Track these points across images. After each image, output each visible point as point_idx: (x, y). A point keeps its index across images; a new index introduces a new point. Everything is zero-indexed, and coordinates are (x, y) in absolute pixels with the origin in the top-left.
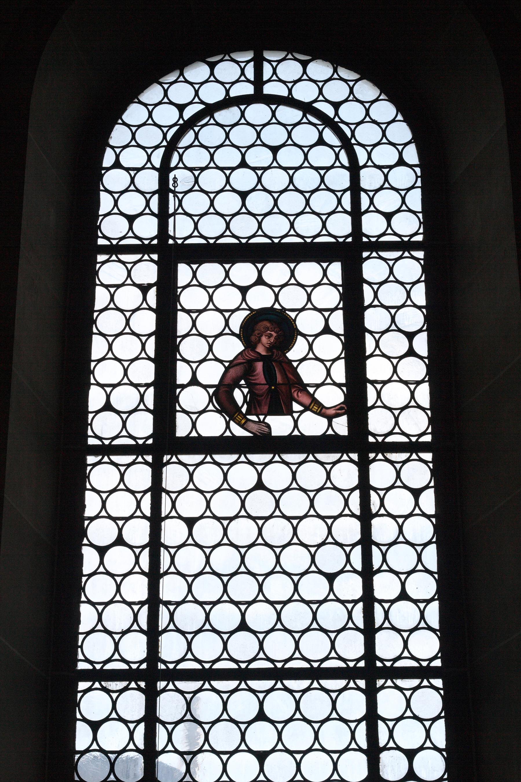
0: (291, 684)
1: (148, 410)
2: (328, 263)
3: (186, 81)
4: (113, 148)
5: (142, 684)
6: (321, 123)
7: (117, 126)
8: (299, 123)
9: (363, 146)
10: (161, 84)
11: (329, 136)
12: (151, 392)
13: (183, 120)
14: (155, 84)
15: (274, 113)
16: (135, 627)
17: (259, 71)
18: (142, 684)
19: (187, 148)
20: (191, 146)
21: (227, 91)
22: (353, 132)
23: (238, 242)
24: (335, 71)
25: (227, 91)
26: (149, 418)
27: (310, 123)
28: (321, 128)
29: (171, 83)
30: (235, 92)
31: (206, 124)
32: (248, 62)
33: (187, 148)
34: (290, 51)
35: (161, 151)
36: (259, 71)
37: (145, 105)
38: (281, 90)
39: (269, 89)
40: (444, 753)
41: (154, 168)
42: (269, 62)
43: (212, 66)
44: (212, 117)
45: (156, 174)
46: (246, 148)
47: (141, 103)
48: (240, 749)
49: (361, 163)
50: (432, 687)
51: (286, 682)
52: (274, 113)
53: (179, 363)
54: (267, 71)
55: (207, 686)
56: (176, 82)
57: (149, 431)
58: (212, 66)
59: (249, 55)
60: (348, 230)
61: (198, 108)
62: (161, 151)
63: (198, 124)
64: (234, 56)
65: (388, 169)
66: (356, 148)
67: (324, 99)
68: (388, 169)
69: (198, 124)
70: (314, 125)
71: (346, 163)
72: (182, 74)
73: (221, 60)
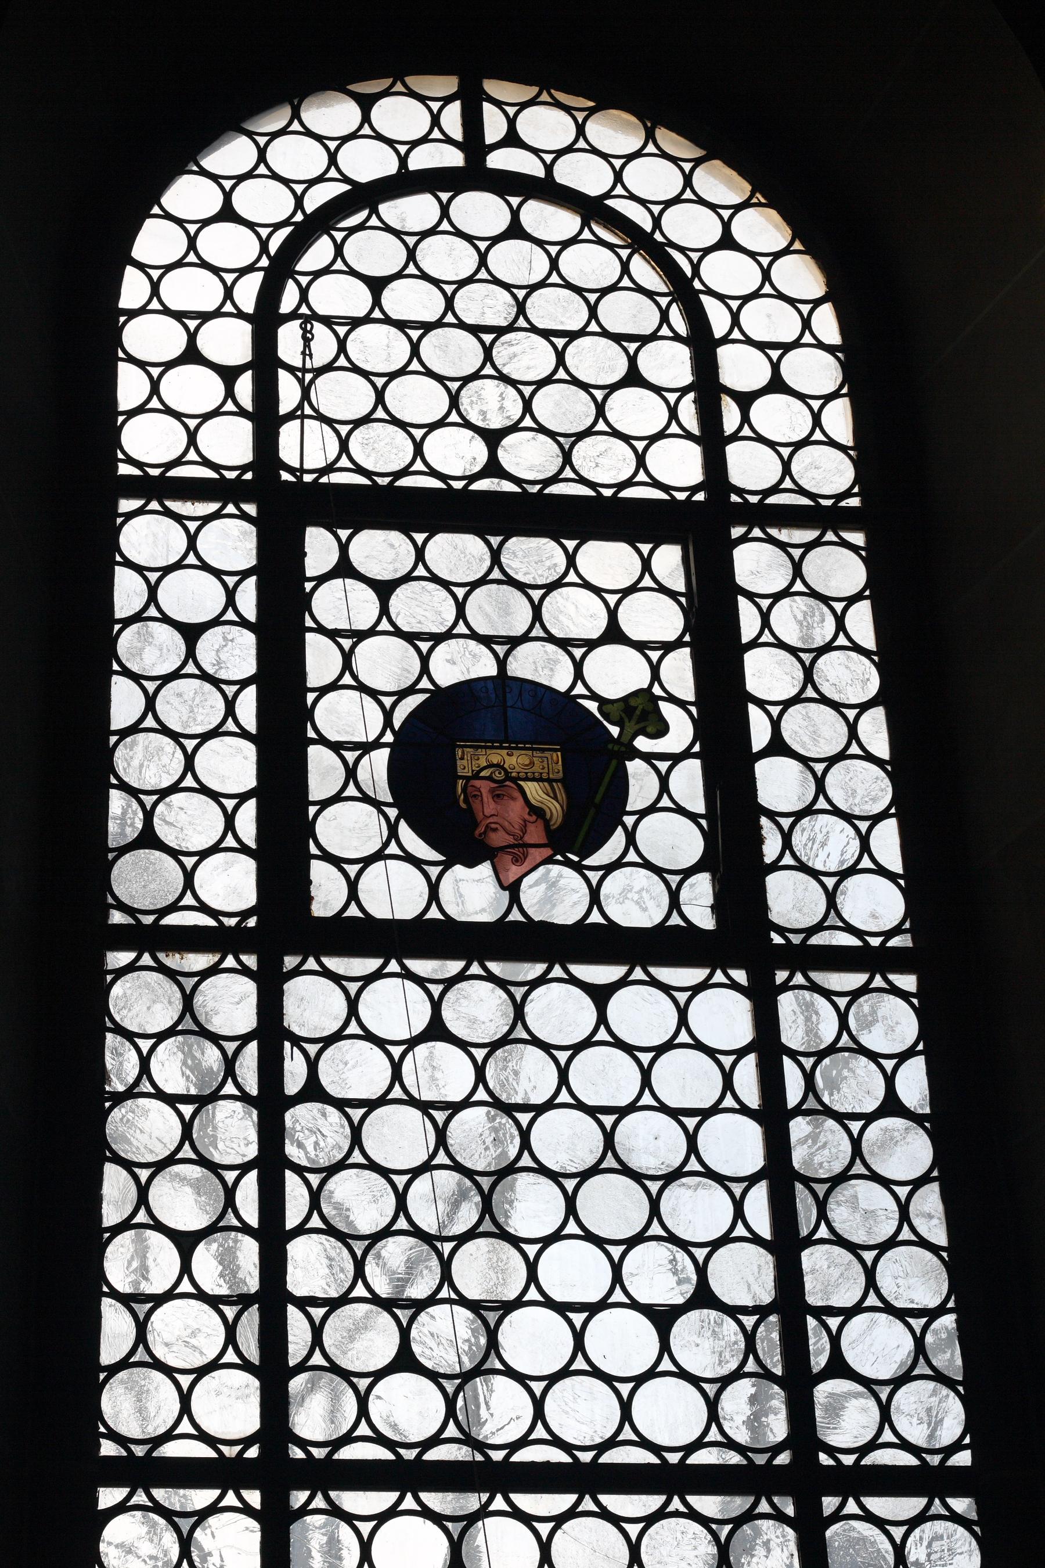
0: (617, 1503)
1: (243, 849)
2: (587, 1314)
3: (308, 133)
4: (141, 267)
5: (254, 1498)
6: (580, 701)
7: (149, 223)
8: (574, 241)
9: (721, 298)
10: (250, 135)
11: (643, 271)
12: (249, 810)
13: (304, 212)
14: (253, 562)
15: (496, 556)
16: (230, 1357)
17: (473, 122)
18: (254, 1498)
19: (317, 274)
20: (326, 271)
21: (403, 160)
22: (696, 268)
23: (444, 486)
24: (650, 136)
25: (403, 160)
26: (247, 867)
27: (600, 242)
28: (624, 253)
29: (274, 135)
30: (421, 160)
31: (361, 227)
32: (447, 100)
33: (317, 274)
34: (544, 86)
35: (257, 278)
36: (473, 122)
37: (215, 178)
38: (529, 166)
39: (499, 160)
40: (945, 1254)
41: (240, 315)
42: (498, 104)
43: (366, 104)
44: (374, 211)
45: (246, 328)
46: (456, 322)
47: (204, 173)
48: (538, 1246)
49: (719, 332)
50: (895, 991)
51: (605, 1499)
52: (496, 556)
53: (309, 637)
54: (494, 126)
55: (409, 1503)
56: (283, 132)
57: (249, 898)
58: (366, 104)
59: (448, 85)
60: (696, 476)
61: (335, 189)
62: (255, 280)
63: (340, 225)
64: (414, 82)
65: (780, 352)
66: (705, 299)
67: (508, 1509)
68: (780, 352)
69: (340, 225)
70: (611, 247)
71: (682, 329)
72: (296, 115)
73: (386, 93)
